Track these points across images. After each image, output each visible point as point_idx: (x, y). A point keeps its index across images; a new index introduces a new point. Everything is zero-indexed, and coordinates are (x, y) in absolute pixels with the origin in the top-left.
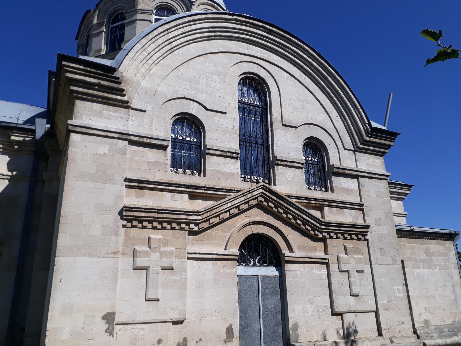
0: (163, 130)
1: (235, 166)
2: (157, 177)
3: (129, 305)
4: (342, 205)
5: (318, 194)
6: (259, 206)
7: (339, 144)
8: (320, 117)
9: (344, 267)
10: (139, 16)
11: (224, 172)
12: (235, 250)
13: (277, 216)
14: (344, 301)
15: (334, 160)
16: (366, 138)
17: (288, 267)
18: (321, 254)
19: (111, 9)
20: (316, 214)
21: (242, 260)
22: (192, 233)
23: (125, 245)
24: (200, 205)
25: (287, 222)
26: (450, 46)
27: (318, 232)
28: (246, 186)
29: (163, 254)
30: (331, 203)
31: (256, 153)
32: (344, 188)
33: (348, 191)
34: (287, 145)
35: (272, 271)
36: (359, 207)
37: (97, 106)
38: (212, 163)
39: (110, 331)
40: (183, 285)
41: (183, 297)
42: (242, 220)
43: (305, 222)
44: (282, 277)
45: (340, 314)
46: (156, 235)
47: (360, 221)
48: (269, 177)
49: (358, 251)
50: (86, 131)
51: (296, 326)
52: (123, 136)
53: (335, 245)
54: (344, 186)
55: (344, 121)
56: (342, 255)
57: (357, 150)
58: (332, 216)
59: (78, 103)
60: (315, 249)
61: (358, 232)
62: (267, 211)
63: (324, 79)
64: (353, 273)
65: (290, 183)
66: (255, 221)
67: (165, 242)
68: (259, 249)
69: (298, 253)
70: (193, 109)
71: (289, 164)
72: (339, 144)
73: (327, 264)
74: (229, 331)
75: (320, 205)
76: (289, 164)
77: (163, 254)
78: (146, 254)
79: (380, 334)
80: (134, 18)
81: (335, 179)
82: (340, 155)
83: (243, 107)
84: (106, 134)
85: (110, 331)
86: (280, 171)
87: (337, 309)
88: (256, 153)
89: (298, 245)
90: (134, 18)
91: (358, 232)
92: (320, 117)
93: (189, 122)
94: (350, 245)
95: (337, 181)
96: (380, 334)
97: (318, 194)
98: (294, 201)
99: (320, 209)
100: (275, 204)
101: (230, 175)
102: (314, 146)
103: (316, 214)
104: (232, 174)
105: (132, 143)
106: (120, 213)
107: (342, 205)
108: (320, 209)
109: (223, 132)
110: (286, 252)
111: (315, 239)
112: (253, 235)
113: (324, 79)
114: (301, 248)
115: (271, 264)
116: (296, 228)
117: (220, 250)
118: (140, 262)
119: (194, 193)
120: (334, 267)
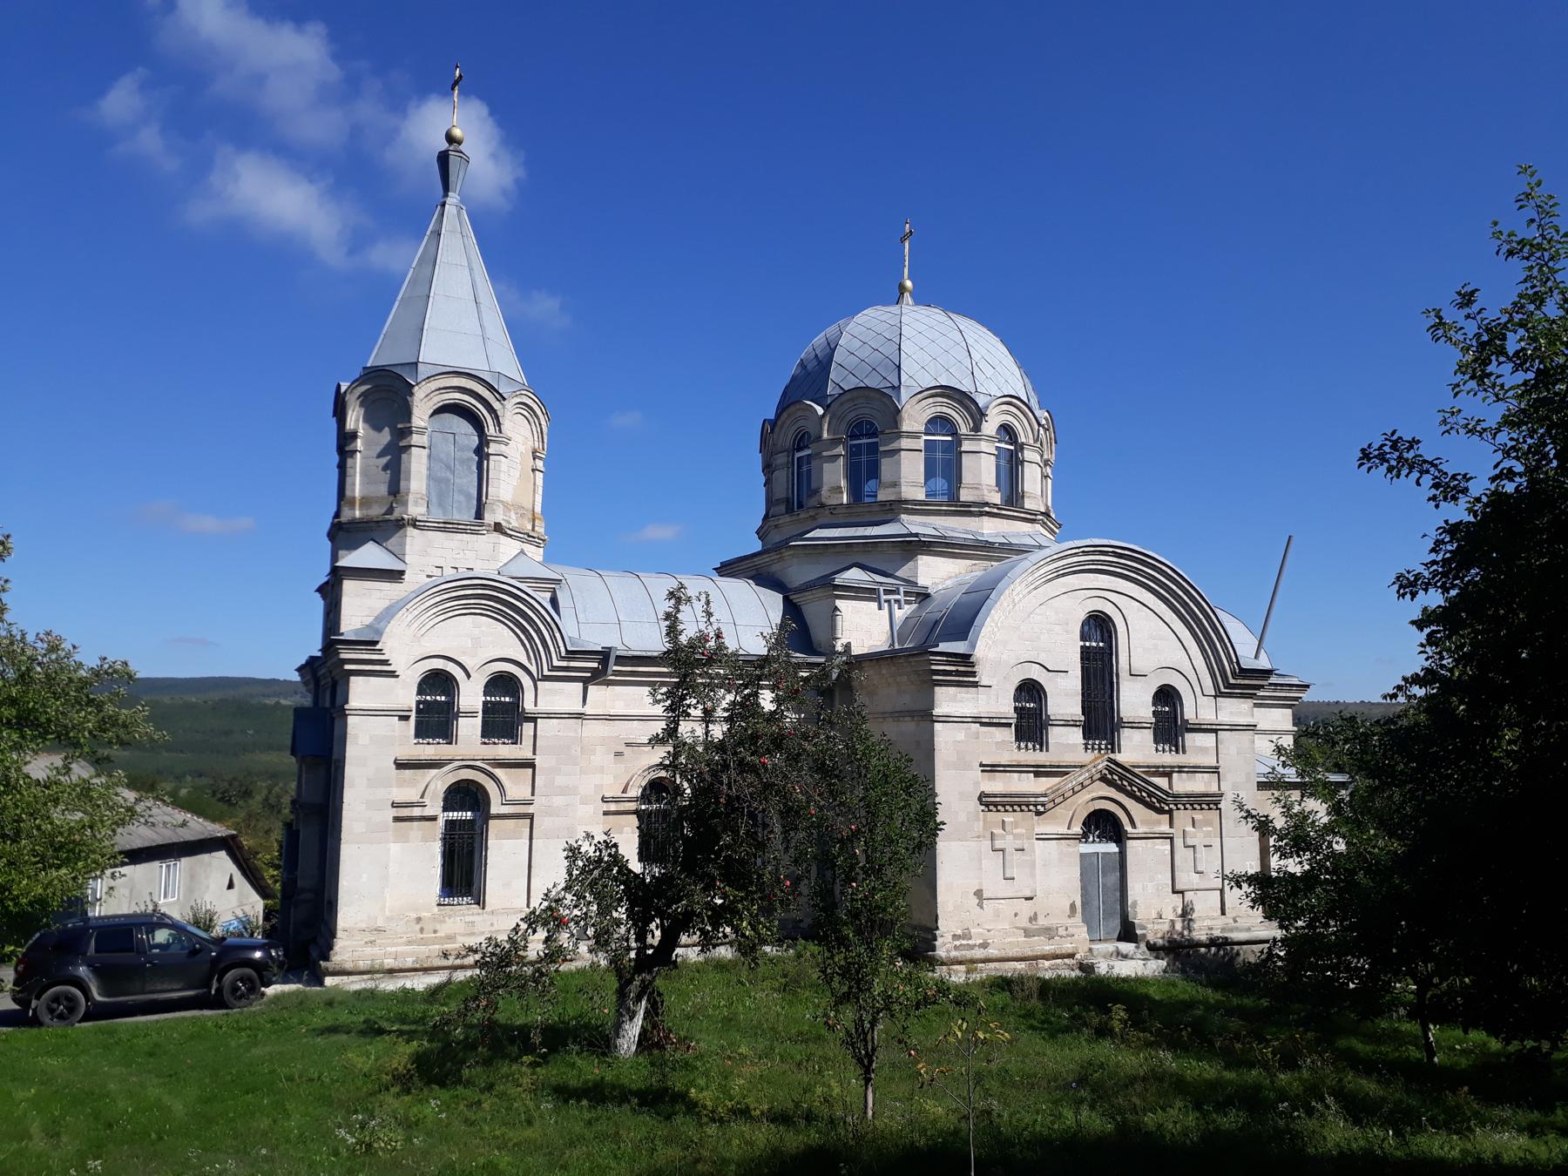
0: (1004, 704)
1: (1076, 735)
2: (1005, 758)
3: (994, 885)
4: (1195, 770)
5: (1168, 758)
6: (1103, 779)
7: (1198, 690)
8: (1177, 658)
9: (1190, 842)
10: (905, 443)
11: (1067, 743)
12: (1077, 829)
13: (1121, 789)
14: (1186, 879)
15: (1189, 714)
16: (1232, 681)
17: (1130, 843)
18: (1165, 828)
19: (853, 414)
20: (1162, 782)
21: (1084, 837)
22: (1038, 813)
23: (985, 828)
24: (1045, 784)
25: (1131, 795)
26: (1467, 299)
27: (1161, 804)
28: (1089, 757)
29: (1016, 837)
30: (1181, 769)
31: (1100, 720)
32: (1198, 747)
33: (1203, 750)
34: (1135, 701)
35: (1112, 848)
36: (1215, 770)
37: (952, 690)
38: (1055, 735)
39: (980, 905)
40: (1033, 865)
41: (1033, 875)
42: (1085, 796)
43: (1150, 794)
44: (1122, 854)
45: (1182, 892)
46: (1009, 818)
47: (1214, 789)
48: (1113, 746)
49: (1208, 823)
50: (947, 719)
51: (1135, 904)
52: (977, 720)
53: (1182, 816)
54: (1198, 744)
55: (1206, 657)
56: (1189, 829)
57: (1219, 694)
58: (1182, 784)
59: (937, 689)
60: (1159, 823)
61: (1209, 802)
62: (1110, 783)
63: (1184, 605)
64: (1200, 848)
65: (1137, 748)
66: (1097, 796)
67: (1016, 825)
68: (1103, 824)
69: (1141, 829)
70: (1036, 673)
71: (1134, 726)
72: (1198, 690)
73: (1172, 839)
74: (1073, 906)
75: (1167, 773)
76: (1134, 726)
77: (1016, 837)
78: (1003, 837)
79: (1223, 913)
80: (894, 446)
81: (1188, 736)
82: (1199, 707)
83: (1086, 654)
84: (961, 720)
85: (980, 905)
86: (1126, 734)
87: (1178, 887)
88: (1100, 720)
89: (1142, 819)
90: (894, 446)
91: (1209, 802)
92: (1177, 658)
93: (1030, 691)
94: (1198, 816)
95: (1191, 739)
96: (1223, 913)
97: (1168, 758)
98: (1136, 770)
99: (1168, 775)
100: (1119, 777)
101: (1071, 748)
102: (1166, 696)
103: (1162, 782)
104: (1075, 745)
105: (983, 724)
106: (980, 799)
107: (1195, 770)
108: (1168, 775)
109: (1064, 698)
110: (1128, 828)
111: (1160, 811)
112: (1096, 812)
113: (1184, 605)
114: (1144, 822)
115: (1110, 839)
116: (1140, 800)
117: (1063, 830)
118: (998, 844)
119: (1039, 772)
120: (1178, 842)
